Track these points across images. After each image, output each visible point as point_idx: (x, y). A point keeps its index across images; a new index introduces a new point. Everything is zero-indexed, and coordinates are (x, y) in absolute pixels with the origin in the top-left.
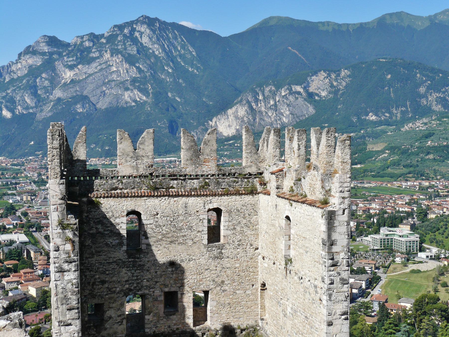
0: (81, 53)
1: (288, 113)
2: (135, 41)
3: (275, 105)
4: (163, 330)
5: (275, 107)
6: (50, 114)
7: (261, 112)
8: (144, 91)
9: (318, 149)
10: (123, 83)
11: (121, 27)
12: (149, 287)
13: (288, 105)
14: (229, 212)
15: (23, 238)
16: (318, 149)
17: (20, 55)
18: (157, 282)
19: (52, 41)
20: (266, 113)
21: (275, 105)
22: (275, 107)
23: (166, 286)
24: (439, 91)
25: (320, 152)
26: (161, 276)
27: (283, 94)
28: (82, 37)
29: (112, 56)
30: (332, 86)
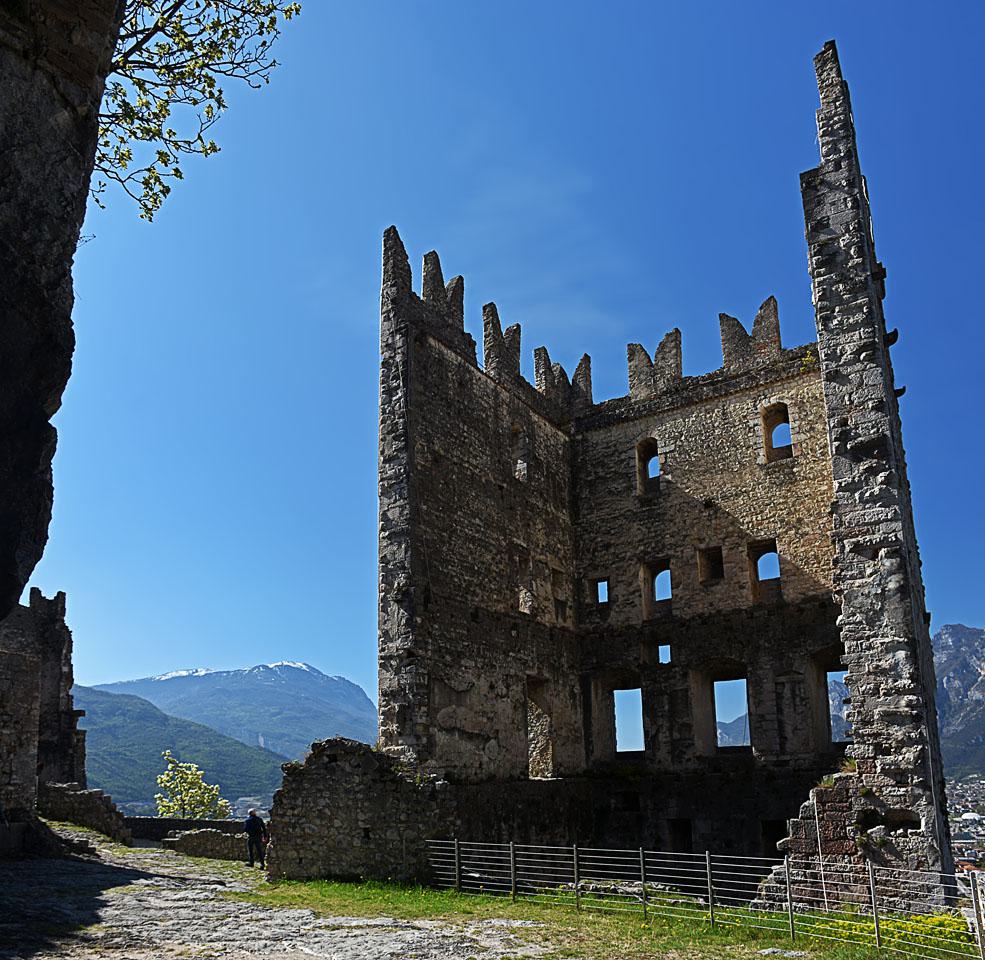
18: (685, 536)
23: (701, 540)
26: (693, 526)
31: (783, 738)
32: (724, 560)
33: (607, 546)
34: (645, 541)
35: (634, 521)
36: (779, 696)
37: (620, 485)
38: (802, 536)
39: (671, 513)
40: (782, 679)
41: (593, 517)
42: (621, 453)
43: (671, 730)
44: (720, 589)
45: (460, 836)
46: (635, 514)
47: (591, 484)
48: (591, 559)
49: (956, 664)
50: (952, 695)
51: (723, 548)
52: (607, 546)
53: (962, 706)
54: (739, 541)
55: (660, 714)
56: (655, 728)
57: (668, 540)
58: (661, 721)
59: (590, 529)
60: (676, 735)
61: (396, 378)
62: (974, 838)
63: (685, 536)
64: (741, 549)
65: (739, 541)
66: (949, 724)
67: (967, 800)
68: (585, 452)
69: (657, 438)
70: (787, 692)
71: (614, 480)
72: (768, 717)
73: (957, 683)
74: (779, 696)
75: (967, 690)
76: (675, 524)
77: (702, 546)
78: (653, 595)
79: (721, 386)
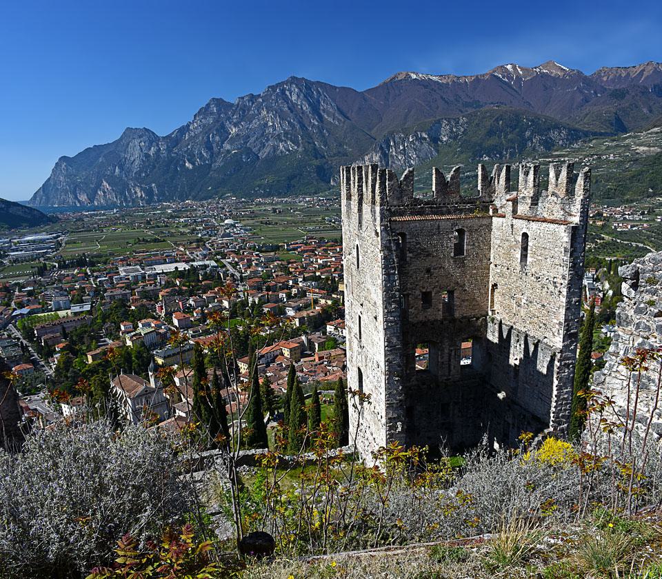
0: (243, 110)
1: (415, 156)
2: (286, 100)
3: (404, 150)
4: (421, 319)
5: (404, 152)
6: (222, 164)
7: (392, 156)
8: (295, 142)
9: (557, 180)
10: (279, 135)
11: (273, 88)
12: (412, 289)
13: (415, 150)
14: (471, 232)
15: (213, 263)
16: (557, 180)
17: (195, 116)
18: (417, 285)
19: (219, 102)
20: (397, 157)
21: (404, 150)
22: (404, 152)
23: (424, 288)
24: (542, 135)
25: (559, 182)
26: (420, 280)
27: (411, 140)
28: (243, 98)
29: (268, 113)
30: (452, 132)
31: (450, 371)
36: (450, 355)
39: (411, 272)
40: (452, 348)
49: (218, 125)
50: (214, 145)
53: (219, 153)
60: (408, 372)
61: (394, 268)
62: (232, 236)
63: (417, 285)
66: (215, 161)
67: (226, 211)
69: (407, 233)
70: (453, 353)
73: (217, 138)
74: (450, 355)
75: (223, 143)
77: (424, 290)
79: (434, 207)
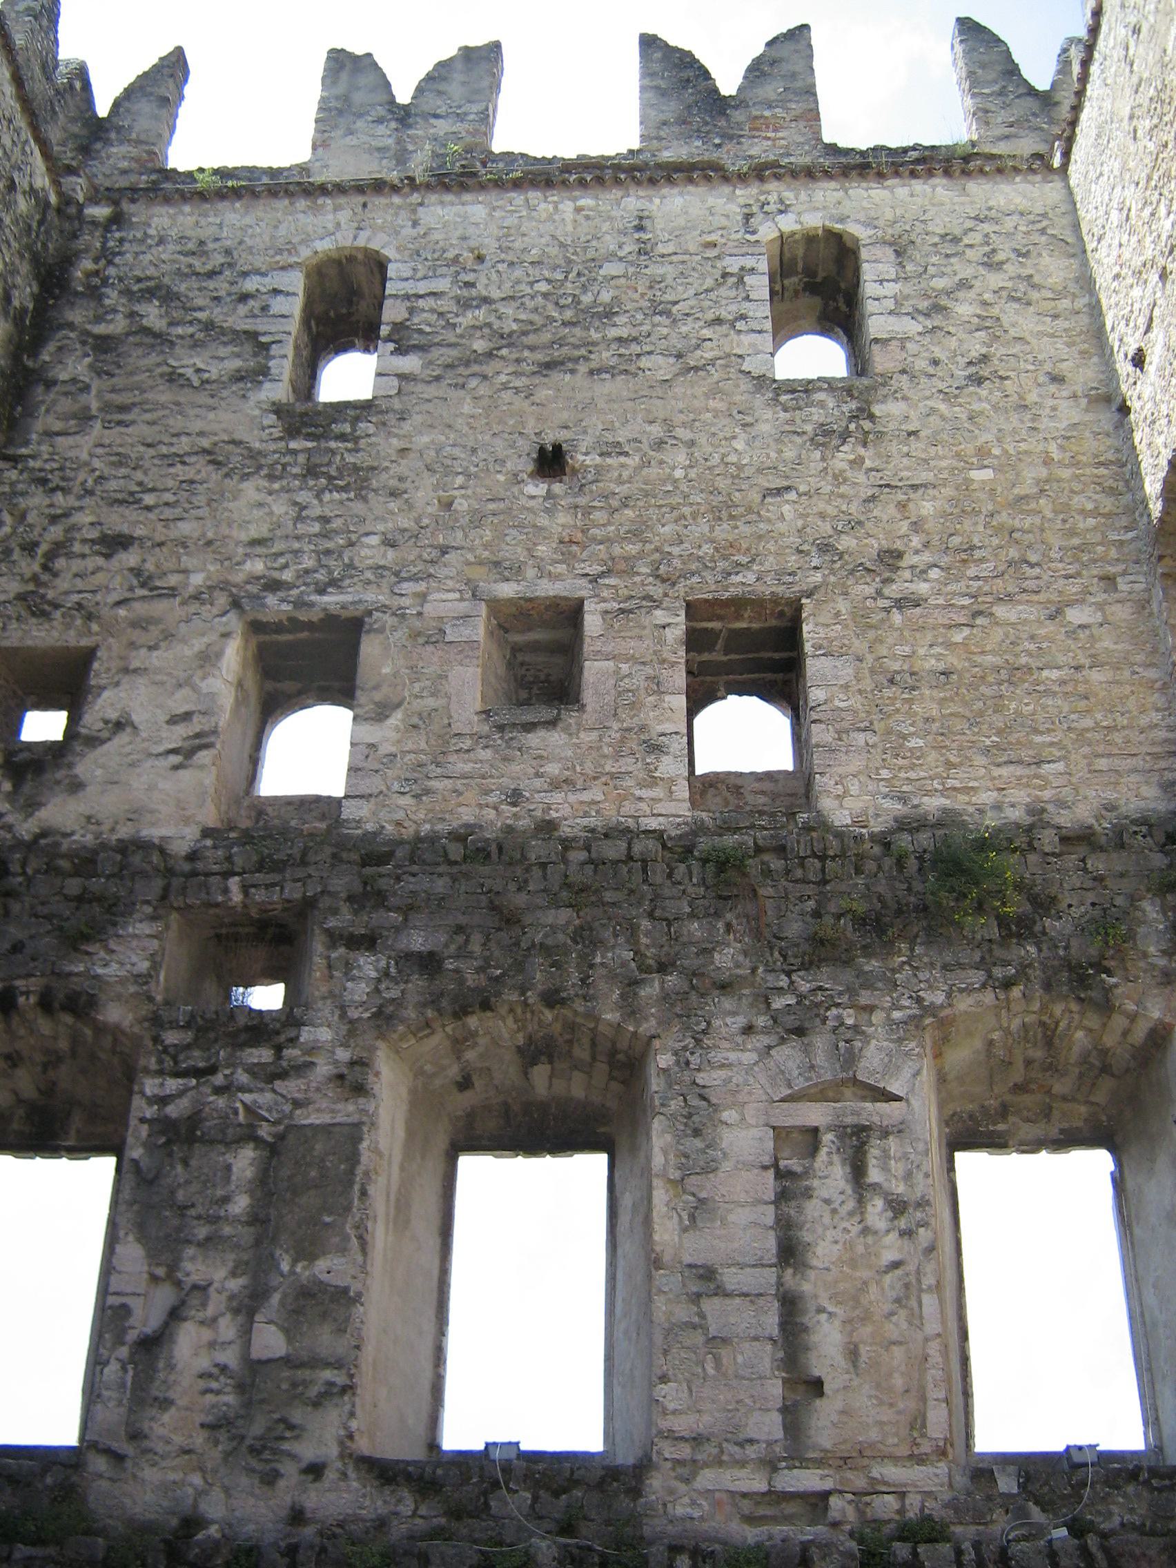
18: (444, 550)
26: (477, 519)
32: (587, 648)
33: (114, 543)
34: (278, 546)
35: (245, 477)
37: (221, 362)
38: (901, 603)
41: (80, 447)
42: (245, 274)
43: (247, 1308)
44: (555, 745)
45: (867, 951)
46: (254, 455)
47: (103, 345)
48: (35, 578)
51: (587, 606)
52: (114, 543)
54: (657, 590)
55: (202, 1232)
56: (164, 1297)
57: (370, 551)
58: (195, 1268)
59: (55, 480)
60: (270, 1341)
63: (444, 550)
64: (660, 616)
65: (657, 590)
68: (107, 256)
71: (196, 345)
72: (731, 1278)
76: (410, 506)
78: (252, 777)
